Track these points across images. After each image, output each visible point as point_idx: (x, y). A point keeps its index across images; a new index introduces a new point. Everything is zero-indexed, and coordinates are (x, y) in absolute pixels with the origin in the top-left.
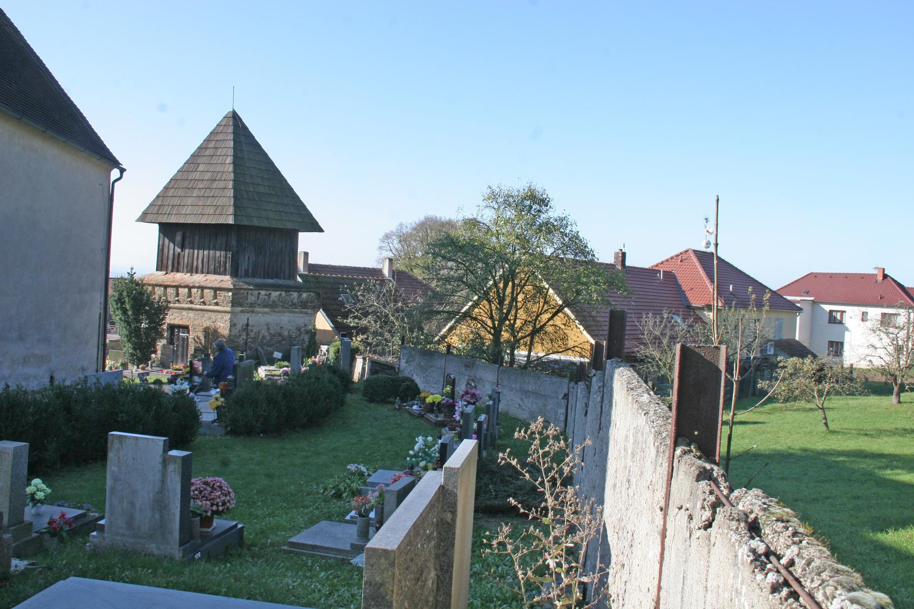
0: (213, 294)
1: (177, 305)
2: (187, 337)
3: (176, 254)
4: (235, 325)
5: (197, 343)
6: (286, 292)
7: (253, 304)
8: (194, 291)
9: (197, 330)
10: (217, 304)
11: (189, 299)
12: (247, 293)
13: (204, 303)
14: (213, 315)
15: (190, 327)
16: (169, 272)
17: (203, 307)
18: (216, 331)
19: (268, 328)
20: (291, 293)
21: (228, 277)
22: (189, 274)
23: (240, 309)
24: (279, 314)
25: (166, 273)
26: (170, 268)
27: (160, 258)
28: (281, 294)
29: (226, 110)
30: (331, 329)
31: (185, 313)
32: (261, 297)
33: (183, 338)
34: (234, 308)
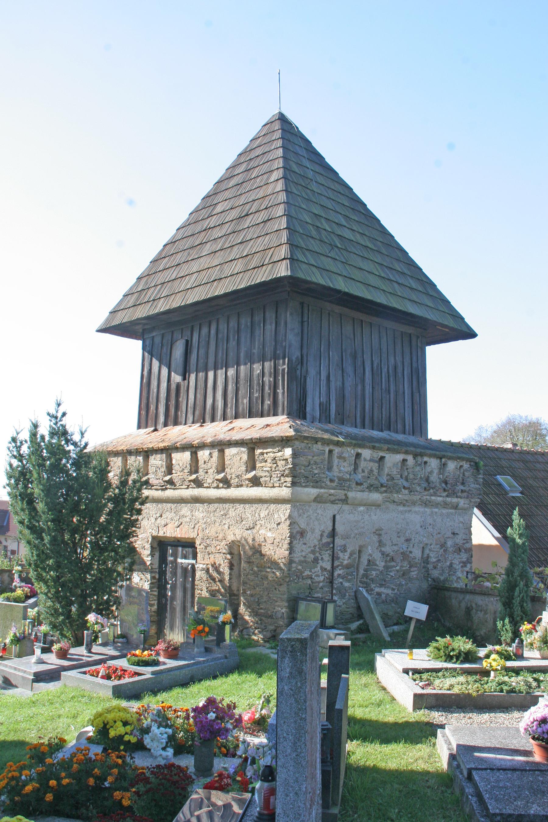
0: (245, 457)
1: (170, 493)
2: (193, 565)
3: (173, 386)
4: (302, 533)
5: (214, 579)
6: (415, 456)
7: (345, 480)
8: (203, 455)
9: (212, 549)
10: (256, 482)
11: (194, 476)
12: (330, 451)
13: (226, 483)
14: (249, 510)
15: (198, 542)
16: (159, 427)
17: (223, 493)
18: (257, 551)
19: (380, 542)
20: (426, 459)
21: (282, 418)
22: (199, 424)
23: (313, 492)
24: (401, 508)
25: (156, 430)
26: (162, 419)
27: (144, 401)
28: (404, 461)
29: (271, 112)
30: (495, 542)
31: (185, 509)
32: (362, 464)
33: (185, 570)
34: (299, 489)
